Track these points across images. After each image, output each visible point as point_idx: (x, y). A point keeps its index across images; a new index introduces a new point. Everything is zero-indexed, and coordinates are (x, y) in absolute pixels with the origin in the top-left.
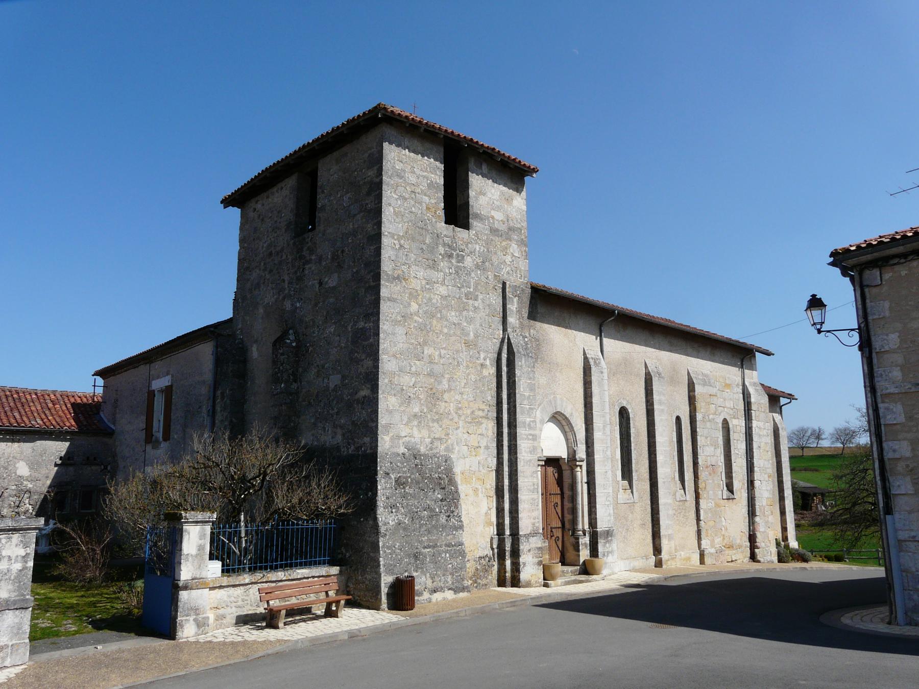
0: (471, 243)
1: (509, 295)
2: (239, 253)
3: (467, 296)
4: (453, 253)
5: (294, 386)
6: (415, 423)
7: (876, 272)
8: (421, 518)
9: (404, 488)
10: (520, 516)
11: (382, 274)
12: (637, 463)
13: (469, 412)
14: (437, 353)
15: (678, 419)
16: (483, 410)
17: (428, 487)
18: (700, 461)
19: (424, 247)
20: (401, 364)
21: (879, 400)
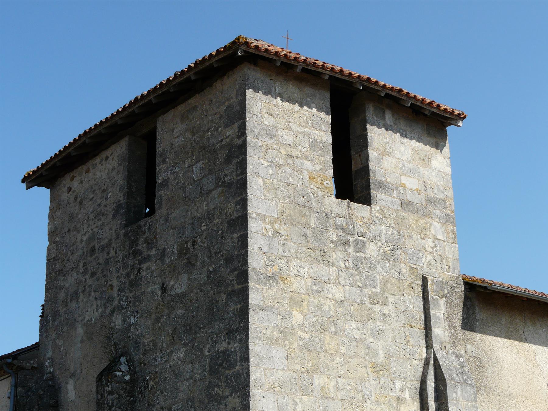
1: (432, 295)
2: (49, 250)
4: (351, 239)
11: (251, 274)
14: (333, 383)
19: (308, 232)
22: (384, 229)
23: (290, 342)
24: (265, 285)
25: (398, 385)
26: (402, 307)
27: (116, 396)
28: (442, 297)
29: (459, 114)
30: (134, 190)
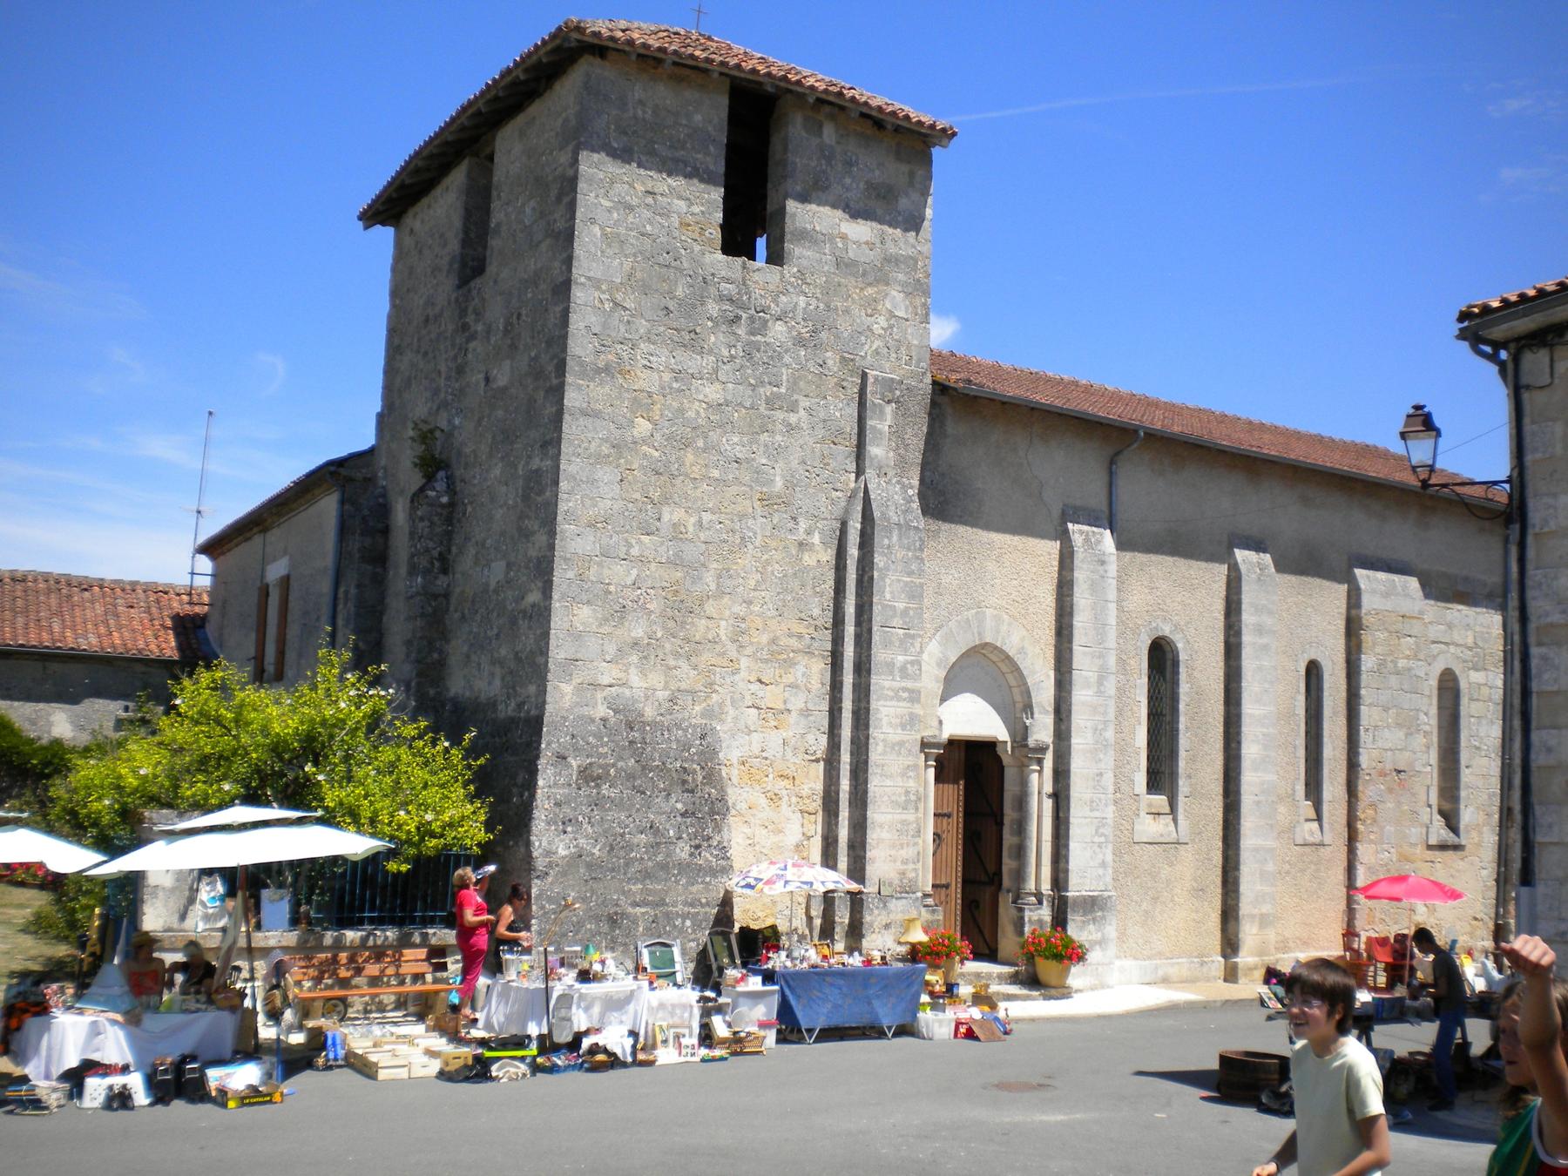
0: (785, 292)
1: (873, 398)
2: (389, 317)
3: (770, 402)
4: (742, 314)
5: (442, 581)
6: (634, 658)
7: (1542, 356)
8: (630, 847)
9: (598, 786)
10: (868, 854)
11: (570, 363)
12: (1193, 759)
13: (764, 639)
14: (692, 520)
15: (1313, 672)
16: (800, 637)
17: (655, 786)
18: (1364, 760)
19: (672, 305)
20: (605, 541)
21: (1532, 639)
22: (802, 301)
23: (627, 462)
24: (592, 379)
25: (803, 525)
26: (822, 415)
27: (427, 523)
28: (889, 402)
29: (944, 130)
30: (472, 235)
